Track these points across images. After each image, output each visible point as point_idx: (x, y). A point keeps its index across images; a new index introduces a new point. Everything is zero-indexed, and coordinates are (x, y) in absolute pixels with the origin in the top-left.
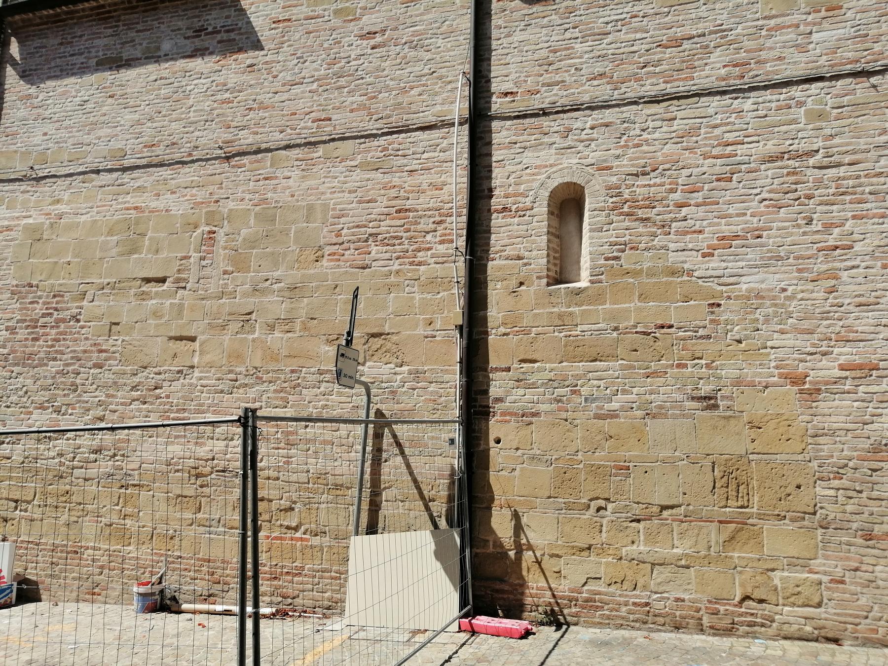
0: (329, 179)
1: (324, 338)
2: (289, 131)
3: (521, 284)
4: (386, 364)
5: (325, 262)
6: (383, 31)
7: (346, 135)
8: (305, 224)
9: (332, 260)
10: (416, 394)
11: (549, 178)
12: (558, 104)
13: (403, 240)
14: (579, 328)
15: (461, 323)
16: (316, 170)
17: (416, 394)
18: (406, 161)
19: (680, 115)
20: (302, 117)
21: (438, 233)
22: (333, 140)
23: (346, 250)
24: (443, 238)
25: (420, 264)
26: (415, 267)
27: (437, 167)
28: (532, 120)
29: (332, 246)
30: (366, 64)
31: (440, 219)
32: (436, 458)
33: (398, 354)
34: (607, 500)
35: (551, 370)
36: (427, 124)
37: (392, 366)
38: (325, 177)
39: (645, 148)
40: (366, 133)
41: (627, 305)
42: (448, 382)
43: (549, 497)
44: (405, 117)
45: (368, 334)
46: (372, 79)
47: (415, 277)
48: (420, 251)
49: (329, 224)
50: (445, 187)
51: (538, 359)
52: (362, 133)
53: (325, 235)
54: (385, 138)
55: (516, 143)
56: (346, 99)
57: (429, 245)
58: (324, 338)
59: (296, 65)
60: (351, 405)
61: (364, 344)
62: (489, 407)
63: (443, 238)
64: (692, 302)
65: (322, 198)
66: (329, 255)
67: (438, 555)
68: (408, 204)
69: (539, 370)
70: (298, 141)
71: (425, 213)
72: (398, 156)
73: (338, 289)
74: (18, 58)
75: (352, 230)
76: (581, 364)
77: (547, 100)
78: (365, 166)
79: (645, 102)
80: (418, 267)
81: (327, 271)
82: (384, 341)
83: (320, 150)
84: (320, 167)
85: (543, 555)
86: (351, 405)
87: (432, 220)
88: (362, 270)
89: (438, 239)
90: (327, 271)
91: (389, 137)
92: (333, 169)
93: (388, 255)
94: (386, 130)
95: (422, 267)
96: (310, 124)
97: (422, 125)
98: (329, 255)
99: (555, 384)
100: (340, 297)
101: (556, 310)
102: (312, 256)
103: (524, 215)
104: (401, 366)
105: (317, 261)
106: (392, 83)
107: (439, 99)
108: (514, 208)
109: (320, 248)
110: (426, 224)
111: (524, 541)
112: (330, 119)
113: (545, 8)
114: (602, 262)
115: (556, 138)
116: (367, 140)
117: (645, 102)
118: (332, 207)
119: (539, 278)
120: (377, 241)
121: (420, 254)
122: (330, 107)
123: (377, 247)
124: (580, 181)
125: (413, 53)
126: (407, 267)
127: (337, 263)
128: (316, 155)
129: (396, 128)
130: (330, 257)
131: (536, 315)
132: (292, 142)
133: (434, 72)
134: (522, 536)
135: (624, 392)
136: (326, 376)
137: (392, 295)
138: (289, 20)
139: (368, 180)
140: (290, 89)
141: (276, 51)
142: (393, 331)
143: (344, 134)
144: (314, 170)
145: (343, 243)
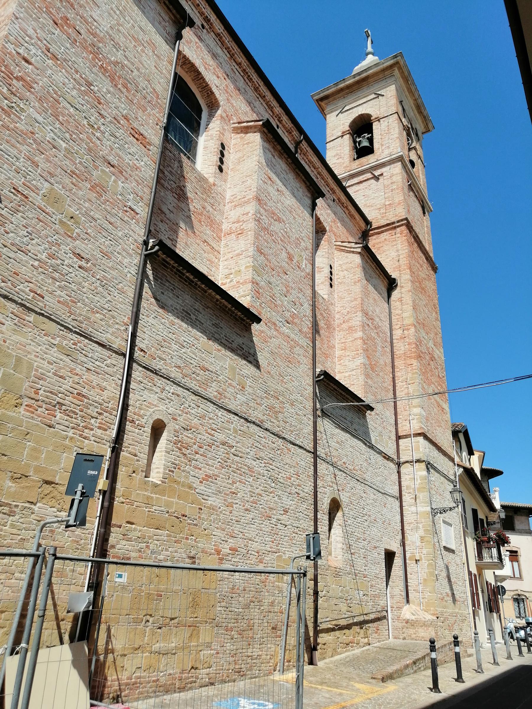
0: (34, 344)
1: (10, 474)
2: (9, 284)
3: (134, 472)
4: (51, 507)
5: (22, 410)
6: (88, 261)
7: (52, 317)
8: (12, 371)
9: (28, 411)
10: (67, 535)
11: (154, 412)
12: (162, 371)
13: (78, 416)
14: (154, 507)
15: (106, 489)
16: (26, 331)
17: (67, 535)
18: (86, 360)
19: (202, 406)
20: (23, 281)
21: (98, 421)
22: (43, 315)
23: (39, 407)
24: (100, 425)
25: (85, 438)
26: (82, 439)
27: (103, 374)
28: (151, 374)
29: (30, 399)
30: (73, 275)
31: (101, 411)
32: (72, 586)
33: (61, 501)
34: (151, 615)
35: (140, 531)
36: (102, 343)
37: (55, 510)
38: (31, 340)
39: (188, 415)
40: (65, 324)
41: (172, 500)
42: (87, 529)
43: (127, 615)
44: (90, 329)
45: (44, 480)
46: (75, 288)
47: (81, 447)
48: (86, 429)
49: (31, 381)
50: (105, 391)
51: (135, 523)
52: (63, 323)
53: (25, 387)
54: (77, 336)
55: (142, 383)
56: (56, 290)
57: (92, 427)
58: (10, 474)
59: (25, 237)
60: (20, 537)
61: (39, 488)
62: (107, 551)
63: (100, 425)
64: (194, 505)
65: (29, 356)
66: (26, 406)
67: (75, 663)
68: (85, 391)
69: (135, 530)
70: (16, 299)
71: (93, 403)
72: (82, 353)
73: (28, 436)
74: (480, 478)
75: (47, 394)
76: (152, 530)
77: (158, 366)
78: (59, 347)
79: (192, 392)
80: (84, 440)
81: (23, 418)
82: (53, 489)
83: (32, 317)
84: (30, 330)
85: (118, 656)
86: (20, 537)
87: (96, 410)
88: (48, 428)
89: (97, 425)
90: (23, 418)
91: (79, 337)
92: (38, 337)
93: (67, 423)
94: (78, 331)
95: (86, 441)
96: (27, 290)
97: (99, 341)
98: (26, 406)
99: (140, 540)
100: (28, 443)
101: (146, 493)
102: (13, 401)
103: (141, 429)
104: (60, 512)
105: (16, 407)
106: (86, 300)
107: (111, 330)
108: (137, 422)
109: (21, 397)
110: (93, 411)
111: (110, 647)
112: (43, 298)
113: (164, 314)
114: (167, 472)
115: (158, 390)
116: (65, 330)
117: (192, 392)
118: (35, 367)
119: (142, 471)
120: (61, 409)
121: (86, 431)
122: (46, 288)
123: (61, 414)
124: (166, 421)
125: (100, 289)
126: (77, 437)
127: (32, 415)
128: (27, 318)
129: (83, 332)
130: (27, 408)
131: (138, 494)
132: (11, 296)
133: (110, 311)
134: (110, 644)
135: (167, 550)
136: (5, 508)
137: (65, 454)
138: (27, 198)
139: (61, 360)
140: (17, 252)
141: (12, 213)
142: (61, 482)
143: (51, 315)
144: (24, 330)
145: (38, 401)
